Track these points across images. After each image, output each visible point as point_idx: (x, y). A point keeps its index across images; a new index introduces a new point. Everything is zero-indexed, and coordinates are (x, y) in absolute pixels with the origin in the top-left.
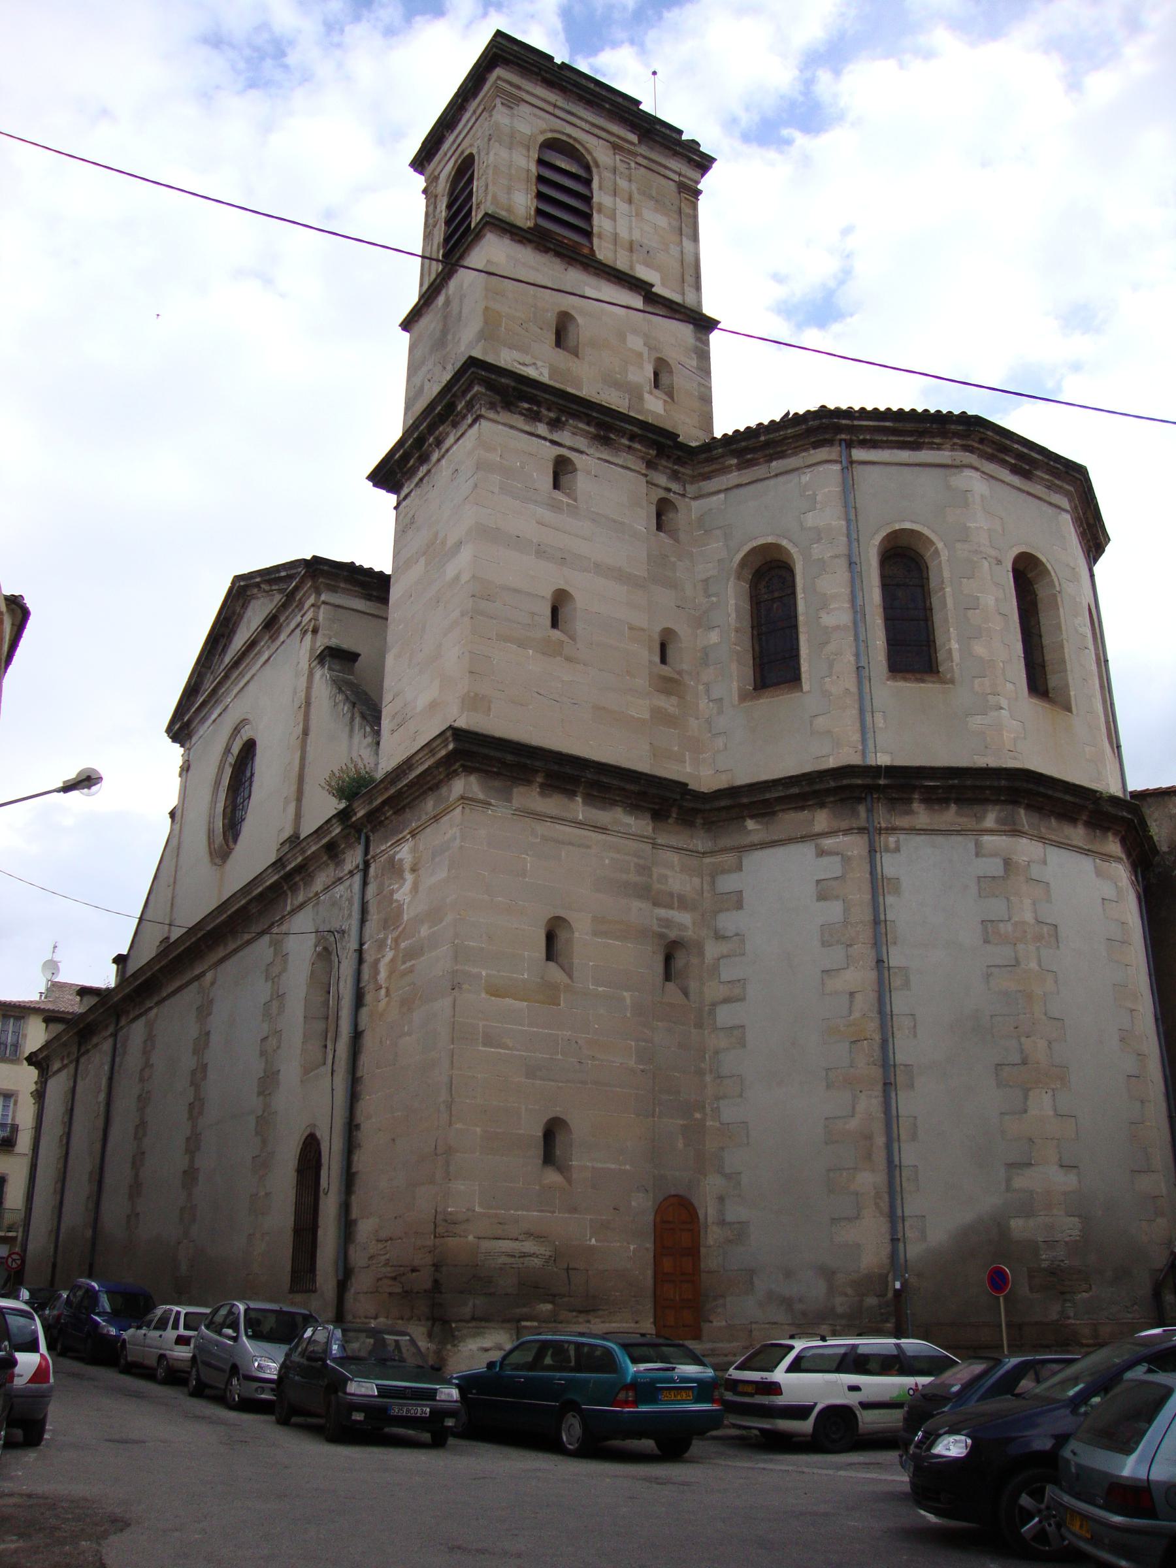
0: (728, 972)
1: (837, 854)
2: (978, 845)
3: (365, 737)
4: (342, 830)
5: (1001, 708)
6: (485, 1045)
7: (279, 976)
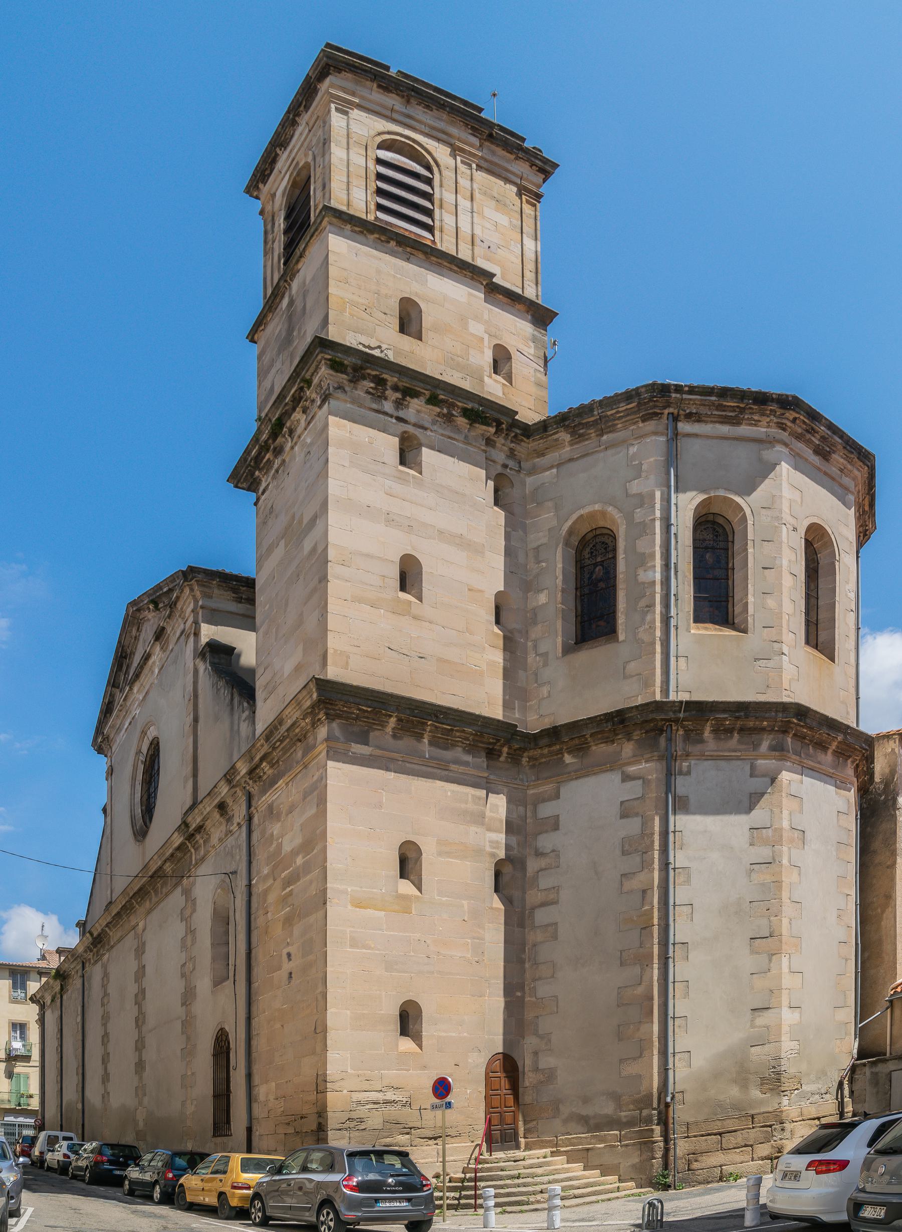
0: (545, 882)
1: (639, 778)
2: (753, 767)
3: (243, 712)
4: (229, 790)
5: (783, 654)
6: (351, 946)
7: (190, 917)
